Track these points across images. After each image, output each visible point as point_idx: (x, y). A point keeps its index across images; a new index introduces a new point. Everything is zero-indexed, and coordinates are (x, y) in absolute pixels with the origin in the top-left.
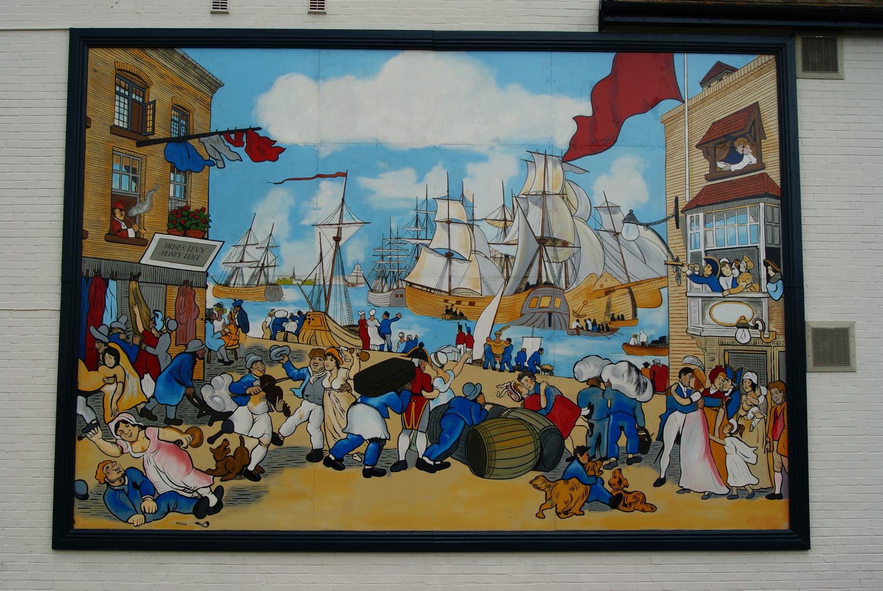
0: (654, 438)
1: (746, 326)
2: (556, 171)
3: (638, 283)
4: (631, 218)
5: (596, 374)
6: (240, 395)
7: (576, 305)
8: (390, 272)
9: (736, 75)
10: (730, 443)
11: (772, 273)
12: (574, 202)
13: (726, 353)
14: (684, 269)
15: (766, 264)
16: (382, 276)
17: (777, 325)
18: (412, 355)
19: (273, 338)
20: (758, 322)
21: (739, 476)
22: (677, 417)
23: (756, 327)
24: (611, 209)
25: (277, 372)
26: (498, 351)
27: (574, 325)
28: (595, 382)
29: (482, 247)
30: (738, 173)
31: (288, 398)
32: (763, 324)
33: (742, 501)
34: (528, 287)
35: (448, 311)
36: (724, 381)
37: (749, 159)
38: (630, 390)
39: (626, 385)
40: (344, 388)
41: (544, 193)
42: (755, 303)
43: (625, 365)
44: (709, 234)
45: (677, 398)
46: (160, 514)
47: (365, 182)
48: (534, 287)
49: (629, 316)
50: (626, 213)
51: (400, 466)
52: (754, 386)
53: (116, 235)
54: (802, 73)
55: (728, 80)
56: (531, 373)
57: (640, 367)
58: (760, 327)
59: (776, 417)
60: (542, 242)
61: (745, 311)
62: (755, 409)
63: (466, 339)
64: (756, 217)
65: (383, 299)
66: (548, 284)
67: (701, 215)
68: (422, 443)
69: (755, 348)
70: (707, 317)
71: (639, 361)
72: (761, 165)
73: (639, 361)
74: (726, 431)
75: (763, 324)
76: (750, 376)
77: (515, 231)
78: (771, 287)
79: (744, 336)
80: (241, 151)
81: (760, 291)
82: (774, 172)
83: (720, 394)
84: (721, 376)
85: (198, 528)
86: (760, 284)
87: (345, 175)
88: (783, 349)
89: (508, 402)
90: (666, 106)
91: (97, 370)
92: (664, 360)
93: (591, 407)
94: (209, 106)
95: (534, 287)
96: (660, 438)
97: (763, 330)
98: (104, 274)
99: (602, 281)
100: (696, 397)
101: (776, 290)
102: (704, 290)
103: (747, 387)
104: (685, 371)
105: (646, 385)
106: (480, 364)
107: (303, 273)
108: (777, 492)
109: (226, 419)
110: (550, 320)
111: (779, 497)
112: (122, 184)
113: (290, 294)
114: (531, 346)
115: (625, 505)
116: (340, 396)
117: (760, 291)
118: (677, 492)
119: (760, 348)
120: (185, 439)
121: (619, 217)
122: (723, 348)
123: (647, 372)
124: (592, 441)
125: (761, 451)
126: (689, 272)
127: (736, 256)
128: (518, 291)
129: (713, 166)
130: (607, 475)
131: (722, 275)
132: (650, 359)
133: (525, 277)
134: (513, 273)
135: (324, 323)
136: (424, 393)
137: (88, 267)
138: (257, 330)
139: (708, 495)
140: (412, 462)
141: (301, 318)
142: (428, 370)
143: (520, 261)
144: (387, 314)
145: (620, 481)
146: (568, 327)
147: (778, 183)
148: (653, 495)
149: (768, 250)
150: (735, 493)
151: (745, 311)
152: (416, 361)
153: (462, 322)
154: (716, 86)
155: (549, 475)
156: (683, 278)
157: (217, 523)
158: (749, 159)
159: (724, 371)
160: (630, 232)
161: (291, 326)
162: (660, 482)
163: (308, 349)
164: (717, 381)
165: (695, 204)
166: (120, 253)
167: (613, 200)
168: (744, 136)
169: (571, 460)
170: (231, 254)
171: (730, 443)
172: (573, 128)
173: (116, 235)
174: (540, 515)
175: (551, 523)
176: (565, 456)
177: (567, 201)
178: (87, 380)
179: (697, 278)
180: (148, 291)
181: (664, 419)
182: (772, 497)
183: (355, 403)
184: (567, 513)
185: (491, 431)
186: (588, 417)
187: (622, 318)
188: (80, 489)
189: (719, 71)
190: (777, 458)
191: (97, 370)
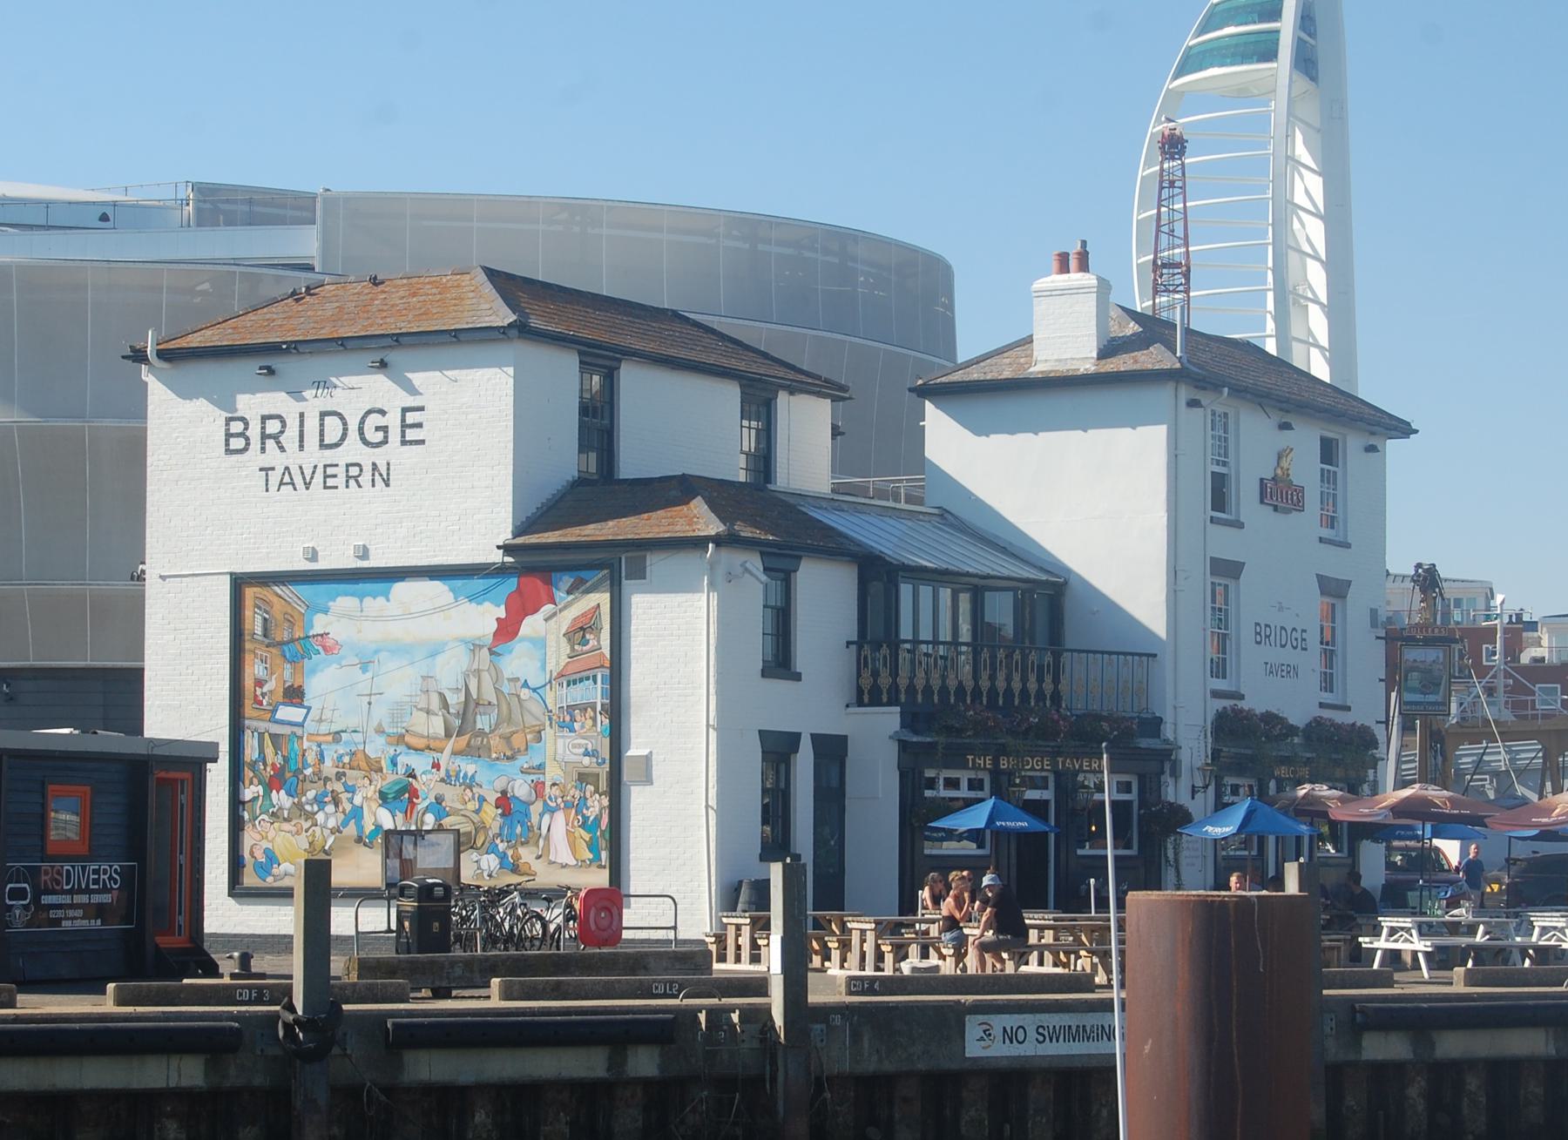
44: (568, 694)
50: (523, 681)
82: (606, 651)
120: (294, 829)
121: (519, 684)
129: (573, 649)
132: (534, 777)
147: (608, 657)
158: (593, 643)
172: (495, 626)
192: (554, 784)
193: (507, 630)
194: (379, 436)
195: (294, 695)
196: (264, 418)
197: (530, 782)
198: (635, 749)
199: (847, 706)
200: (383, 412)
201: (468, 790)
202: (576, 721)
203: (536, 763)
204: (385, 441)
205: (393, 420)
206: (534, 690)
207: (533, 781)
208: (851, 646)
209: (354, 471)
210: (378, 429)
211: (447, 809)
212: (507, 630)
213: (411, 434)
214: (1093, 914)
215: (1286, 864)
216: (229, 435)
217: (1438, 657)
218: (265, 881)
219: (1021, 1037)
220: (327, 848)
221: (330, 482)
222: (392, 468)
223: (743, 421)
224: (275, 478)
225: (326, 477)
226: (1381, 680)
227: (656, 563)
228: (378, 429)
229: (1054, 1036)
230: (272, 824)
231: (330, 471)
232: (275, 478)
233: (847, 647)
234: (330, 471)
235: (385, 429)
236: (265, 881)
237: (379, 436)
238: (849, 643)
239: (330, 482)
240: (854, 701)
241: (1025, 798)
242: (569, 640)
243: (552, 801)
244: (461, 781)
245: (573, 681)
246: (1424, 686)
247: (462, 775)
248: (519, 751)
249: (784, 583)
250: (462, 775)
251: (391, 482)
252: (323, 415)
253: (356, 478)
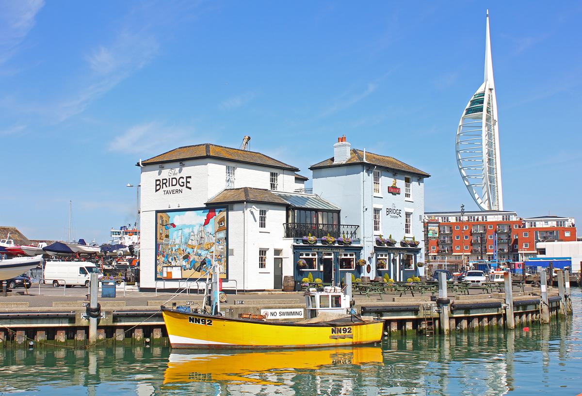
4: (210, 234)
6: (172, 260)
8: (435, 347)
24: (208, 233)
25: (175, 257)
31: (177, 260)
37: (223, 224)
47: (184, 230)
51: (187, 269)
53: (160, 239)
61: (222, 247)
63: (193, 252)
65: (185, 246)
68: (189, 266)
72: (224, 225)
79: (222, 250)
82: (226, 226)
90: (214, 217)
91: (288, 235)
102: (218, 244)
106: (70, 360)
107: (178, 243)
109: (171, 263)
110: (202, 249)
112: (161, 232)
113: (177, 246)
118: (159, 175)
127: (221, 239)
137: (158, 243)
138: (174, 251)
141: (178, 249)
151: (222, 247)
158: (223, 224)
160: (210, 236)
166: (161, 241)
170: (171, 241)
172: (204, 221)
173: (160, 239)
178: (158, 258)
180: (164, 246)
191: (288, 235)
193: (207, 222)
194: (182, 184)
195: (167, 236)
196: (163, 180)
200: (183, 178)
205: (184, 180)
209: (165, 181)
210: (182, 182)
212: (207, 222)
213: (189, 185)
214: (340, 270)
215: (293, 275)
216: (157, 185)
219: (275, 314)
224: (166, 192)
226: (390, 237)
227: (236, 206)
228: (182, 182)
229: (284, 314)
235: (183, 183)
237: (182, 184)
241: (411, 328)
245: (492, 330)
252: (172, 179)
253: (165, 183)
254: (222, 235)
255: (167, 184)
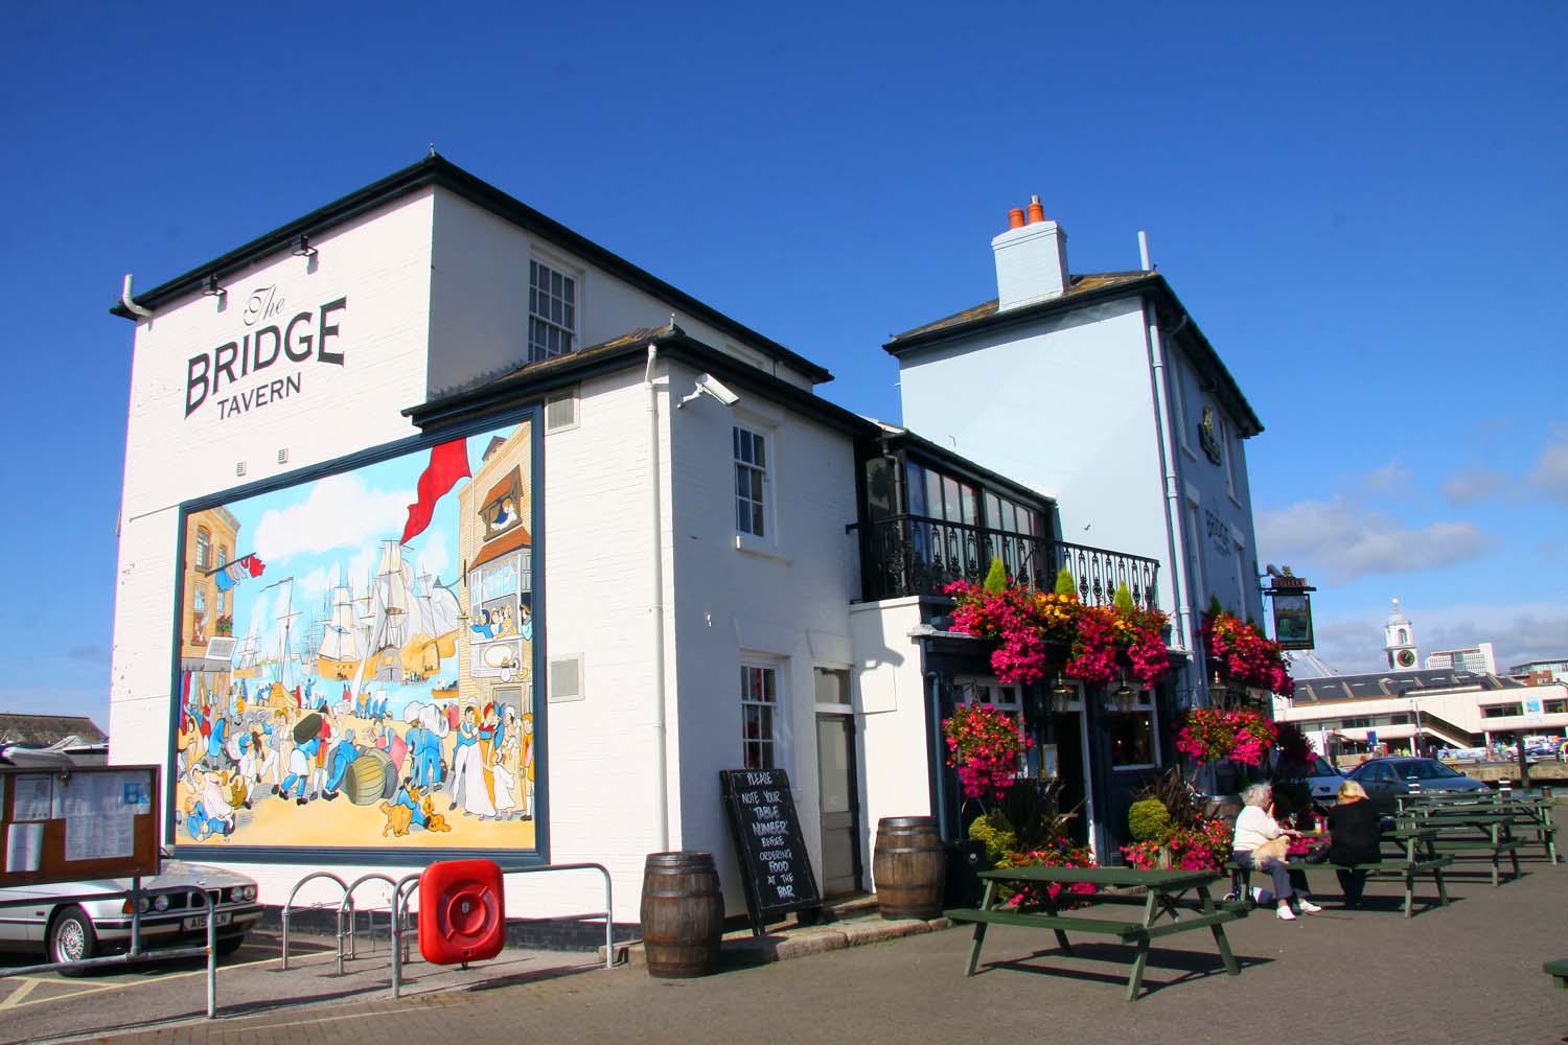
0: (449, 768)
1: (506, 667)
2: (396, 551)
3: (441, 637)
4: (438, 584)
5: (415, 717)
7: (405, 661)
9: (505, 444)
10: (497, 770)
11: (525, 616)
12: (405, 576)
13: (746, 708)
14: (469, 621)
15: (521, 609)
16: (308, 652)
17: (527, 663)
18: (321, 711)
19: (258, 705)
20: (516, 661)
21: (504, 801)
22: (463, 749)
23: (514, 666)
24: (426, 578)
26: (364, 703)
27: (405, 677)
28: (416, 723)
29: (357, 622)
30: (505, 530)
31: (264, 748)
32: (519, 662)
33: (504, 822)
34: (380, 649)
35: (339, 674)
36: (1513, 762)
38: (435, 728)
39: (433, 723)
40: (289, 739)
41: (390, 573)
42: (514, 643)
43: (433, 706)
44: (484, 589)
45: (464, 732)
46: (208, 835)
48: (384, 648)
49: (435, 667)
50: (435, 580)
52: (512, 719)
54: (236, 341)
55: (500, 450)
56: (380, 718)
57: (442, 708)
58: (517, 666)
59: (527, 746)
60: (388, 612)
62: (513, 739)
63: (347, 695)
64: (515, 567)
66: (391, 646)
67: (480, 572)
69: (513, 685)
70: (483, 661)
71: (440, 703)
72: (519, 521)
73: (440, 703)
74: (494, 760)
75: (519, 662)
76: (510, 711)
77: (374, 603)
78: (525, 628)
79: (506, 674)
80: (247, 570)
81: (517, 633)
82: (527, 525)
83: (490, 728)
84: (491, 712)
85: (225, 844)
86: (517, 627)
87: (292, 579)
88: (531, 684)
89: (369, 744)
90: (463, 481)
92: (455, 701)
93: (413, 744)
94: (235, 542)
95: (384, 648)
96: (453, 769)
97: (519, 669)
98: (190, 669)
99: (420, 639)
100: (476, 731)
101: (527, 630)
102: (480, 637)
103: (508, 719)
104: (469, 709)
105: (445, 723)
108: (528, 814)
111: (529, 818)
114: (380, 697)
115: (432, 826)
116: (287, 743)
117: (517, 633)
119: (517, 685)
120: (221, 779)
121: (431, 583)
122: (492, 687)
123: (445, 712)
124: (413, 775)
125: (517, 777)
126: (472, 624)
127: (501, 603)
128: (374, 654)
129: (489, 527)
130: (422, 801)
131: (493, 623)
132: (447, 701)
133: (379, 642)
134: (372, 640)
135: (281, 691)
136: (326, 739)
139: (483, 818)
140: (320, 793)
141: (271, 688)
142: (329, 722)
143: (1450, 737)
144: (309, 680)
145: (429, 806)
146: (401, 677)
147: (530, 532)
148: (451, 817)
149: (523, 595)
150: (500, 815)
152: (323, 714)
153: (346, 682)
154: (492, 457)
155: (390, 801)
156: (468, 628)
157: (237, 839)
158: (512, 517)
159: (493, 707)
160: (438, 594)
161: (266, 695)
162: (454, 806)
163: (273, 710)
164: (489, 716)
165: (477, 565)
167: (428, 572)
168: (509, 497)
169: (401, 788)
171: (497, 770)
174: (385, 834)
175: (392, 842)
176: (398, 787)
177: (402, 577)
179: (477, 628)
181: (455, 751)
182: (526, 818)
183: (294, 749)
184: (399, 833)
185: (361, 768)
186: (411, 752)
187: (431, 669)
188: (178, 818)
189: (498, 441)
190: (528, 782)
192: (469, 709)
194: (304, 347)
195: (224, 626)
197: (442, 708)
198: (555, 652)
199: (852, 603)
200: (306, 316)
201: (378, 723)
202: (493, 623)
203: (445, 684)
204: (308, 353)
206: (447, 588)
207: (445, 706)
208: (851, 531)
210: (303, 340)
211: (358, 748)
216: (192, 384)
217: (1302, 606)
218: (195, 839)
220: (247, 800)
221: (261, 400)
222: (302, 376)
223: (1012, 297)
224: (228, 406)
225: (258, 396)
228: (303, 340)
230: (204, 773)
231: (261, 392)
232: (228, 406)
233: (847, 532)
234: (261, 392)
236: (195, 839)
237: (304, 347)
238: (849, 528)
239: (261, 400)
240: (860, 596)
242: (485, 518)
243: (467, 731)
244: (371, 712)
246: (1293, 630)
247: (372, 705)
248: (431, 669)
249: (712, 900)
250: (372, 705)
251: (301, 389)
254: (509, 577)
255: (237, 368)
